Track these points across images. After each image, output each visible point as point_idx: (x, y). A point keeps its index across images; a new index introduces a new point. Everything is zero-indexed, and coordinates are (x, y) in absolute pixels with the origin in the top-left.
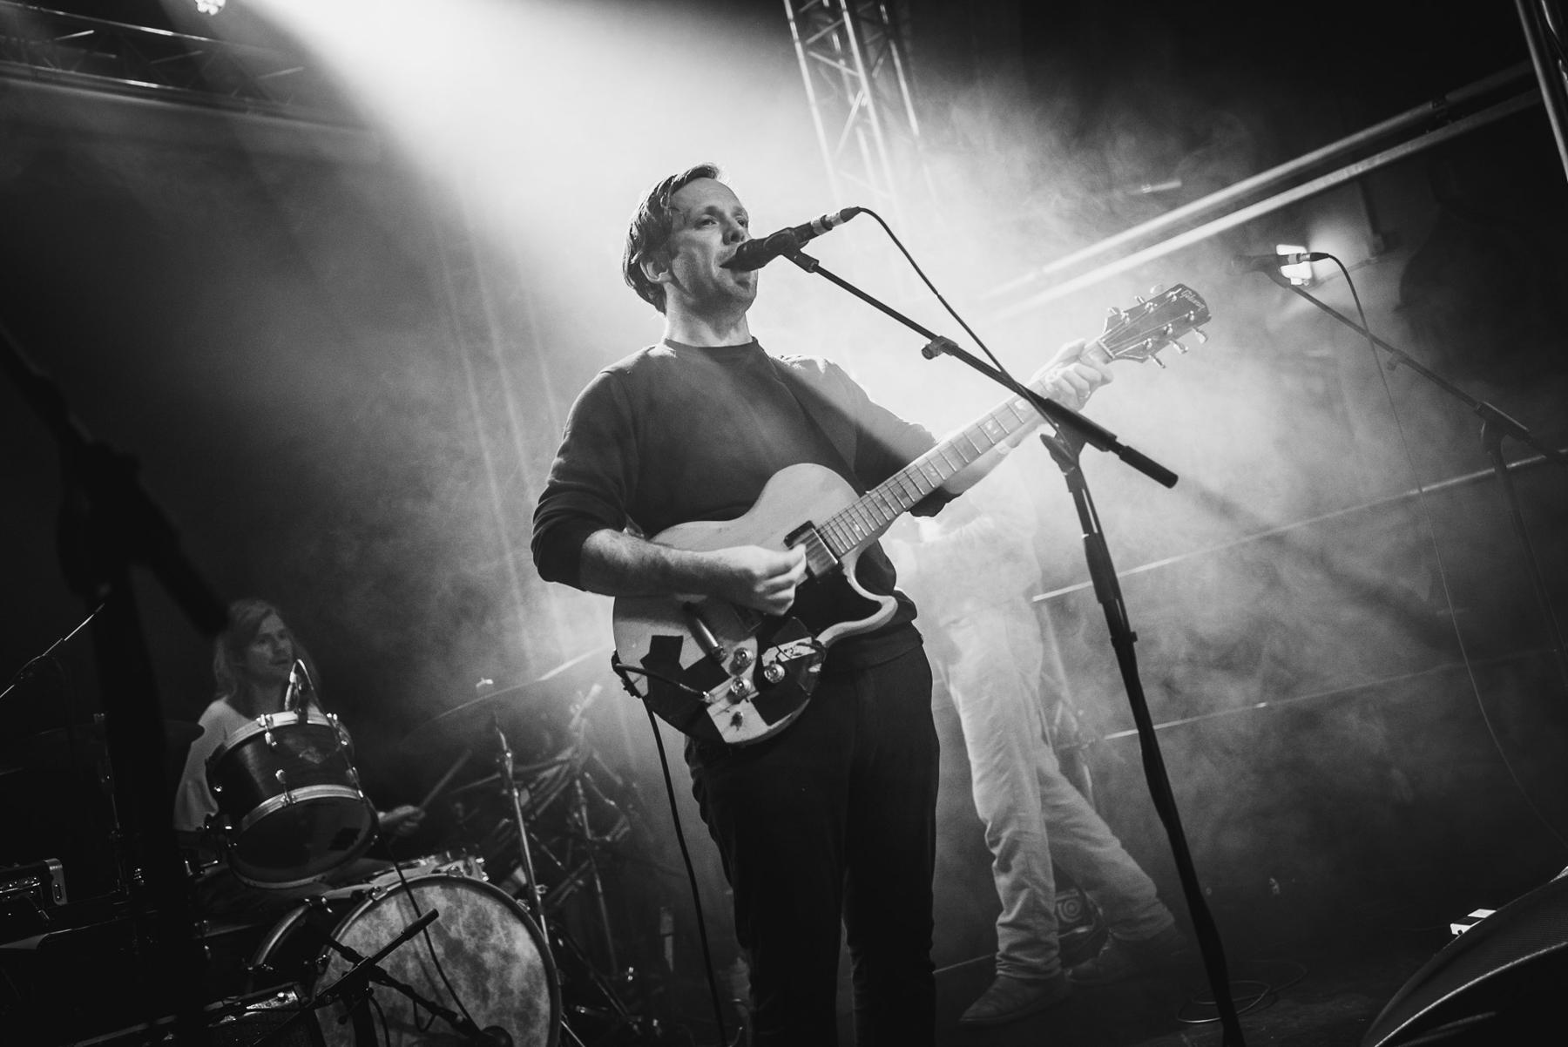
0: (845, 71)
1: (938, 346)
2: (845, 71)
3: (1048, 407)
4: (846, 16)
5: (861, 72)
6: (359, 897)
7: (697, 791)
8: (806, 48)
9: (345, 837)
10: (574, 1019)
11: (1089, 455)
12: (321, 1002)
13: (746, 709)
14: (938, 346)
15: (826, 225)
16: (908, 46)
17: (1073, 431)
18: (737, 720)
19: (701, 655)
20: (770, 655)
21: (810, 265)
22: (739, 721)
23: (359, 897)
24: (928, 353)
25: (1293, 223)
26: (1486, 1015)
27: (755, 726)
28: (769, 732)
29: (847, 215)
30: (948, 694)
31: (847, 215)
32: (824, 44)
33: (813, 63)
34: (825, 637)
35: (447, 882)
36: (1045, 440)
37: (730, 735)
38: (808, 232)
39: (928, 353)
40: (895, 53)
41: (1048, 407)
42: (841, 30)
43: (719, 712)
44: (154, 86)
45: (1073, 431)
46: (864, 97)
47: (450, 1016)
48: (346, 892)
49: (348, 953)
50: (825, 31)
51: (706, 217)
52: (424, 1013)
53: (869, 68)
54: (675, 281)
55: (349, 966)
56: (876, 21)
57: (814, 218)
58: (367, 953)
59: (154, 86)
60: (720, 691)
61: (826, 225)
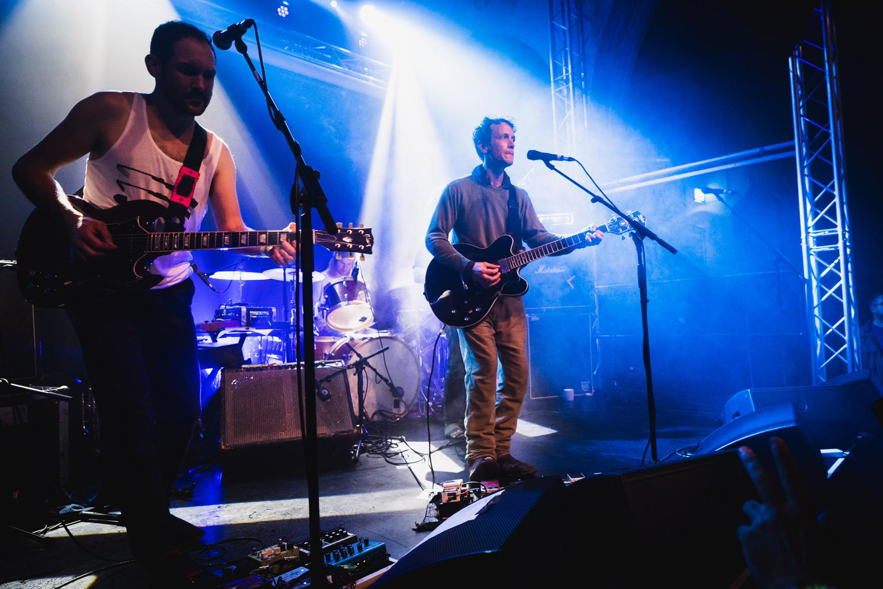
0: (566, 101)
1: (596, 199)
2: (566, 101)
3: (634, 224)
4: (571, 84)
5: (572, 104)
8: (556, 92)
11: (647, 242)
12: (349, 367)
14: (596, 199)
15: (562, 158)
16: (589, 97)
17: (641, 233)
21: (552, 167)
24: (594, 201)
25: (701, 182)
26: (441, 297)
28: (376, 258)
29: (570, 159)
31: (570, 159)
32: (560, 91)
33: (556, 97)
36: (632, 234)
38: (554, 157)
39: (594, 201)
40: (771, 272)
41: (634, 224)
42: (568, 88)
44: (818, 352)
45: (641, 233)
46: (572, 112)
49: (359, 355)
50: (562, 87)
51: (507, 193)
53: (575, 102)
55: (358, 359)
56: (580, 88)
57: (559, 155)
58: (364, 356)
59: (818, 352)
61: (562, 158)
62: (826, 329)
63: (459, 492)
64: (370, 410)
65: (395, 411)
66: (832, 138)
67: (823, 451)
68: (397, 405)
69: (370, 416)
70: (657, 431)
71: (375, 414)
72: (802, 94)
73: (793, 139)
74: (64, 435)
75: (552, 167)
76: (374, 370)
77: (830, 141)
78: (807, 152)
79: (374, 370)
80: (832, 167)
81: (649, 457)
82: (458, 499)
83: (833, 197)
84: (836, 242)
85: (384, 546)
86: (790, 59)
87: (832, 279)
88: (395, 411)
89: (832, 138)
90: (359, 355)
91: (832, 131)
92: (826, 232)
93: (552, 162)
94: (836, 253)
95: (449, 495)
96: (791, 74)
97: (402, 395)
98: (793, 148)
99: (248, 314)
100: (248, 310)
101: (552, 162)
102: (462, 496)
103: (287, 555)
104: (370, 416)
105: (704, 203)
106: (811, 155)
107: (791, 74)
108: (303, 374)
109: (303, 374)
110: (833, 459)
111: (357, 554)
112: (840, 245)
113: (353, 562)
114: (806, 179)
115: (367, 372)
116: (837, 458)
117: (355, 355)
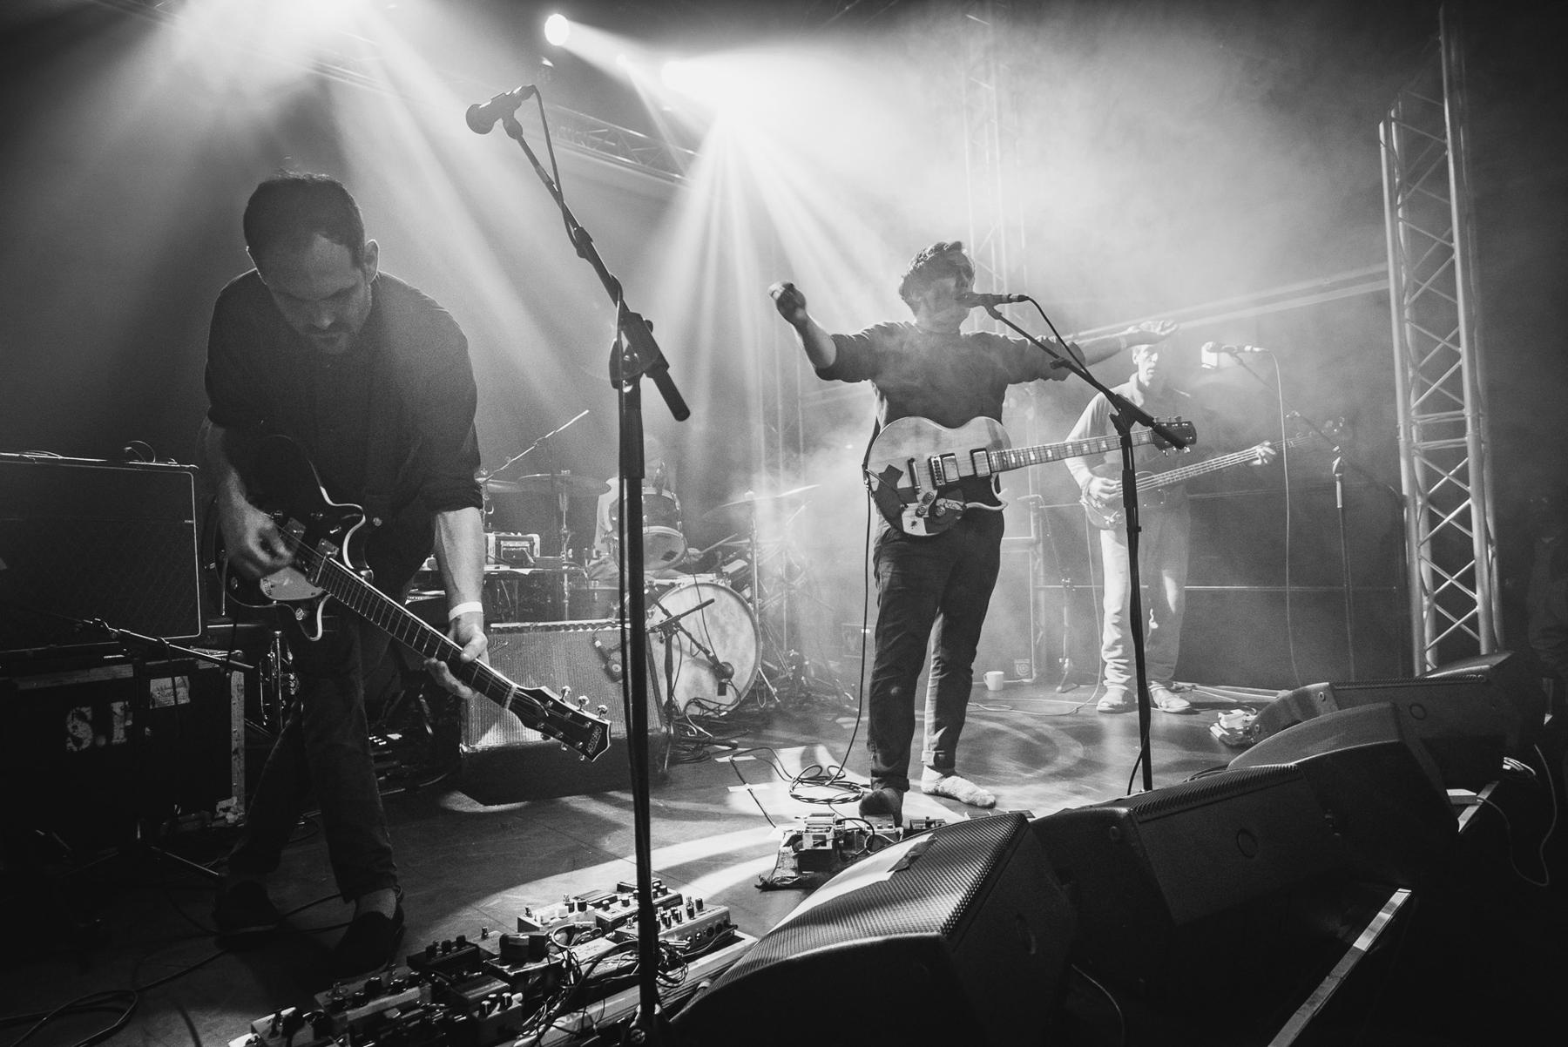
6: (673, 585)
7: (1219, 472)
9: (669, 556)
10: (763, 666)
13: (921, 522)
18: (914, 523)
19: (971, 473)
20: (941, 502)
21: (998, 316)
22: (914, 524)
23: (673, 585)
27: (920, 530)
29: (1022, 298)
30: (1055, 721)
31: (1022, 298)
34: (969, 505)
35: (716, 586)
37: (907, 529)
38: (1000, 300)
43: (907, 518)
47: (707, 652)
48: (667, 582)
49: (665, 612)
52: (696, 649)
54: (925, 301)
55: (664, 618)
58: (674, 614)
60: (912, 507)
62: (1437, 580)
63: (830, 836)
64: (681, 699)
65: (721, 699)
66: (1457, 256)
67: (1451, 792)
68: (722, 692)
69: (682, 707)
70: (652, 801)
71: (689, 703)
72: (1401, 183)
73: (1385, 259)
74: (238, 726)
75: (998, 316)
76: (689, 635)
77: (1453, 262)
78: (1408, 281)
79: (689, 635)
80: (1456, 306)
81: (1138, 788)
82: (829, 846)
83: (1458, 356)
84: (1463, 434)
85: (727, 913)
86: (1381, 126)
87: (1452, 496)
88: (721, 699)
89: (1457, 256)
90: (665, 612)
91: (1456, 244)
92: (1445, 416)
93: (998, 308)
94: (1462, 452)
95: (815, 837)
96: (1383, 150)
97: (730, 676)
98: (1385, 274)
99: (498, 546)
100: (498, 539)
101: (998, 308)
102: (835, 842)
103: (578, 919)
104: (682, 707)
105: (1217, 369)
106: (1417, 287)
107: (1383, 150)
108: (628, 633)
109: (628, 633)
110: (1462, 805)
111: (686, 921)
112: (1469, 438)
113: (682, 934)
114: (1407, 326)
115: (680, 639)
116: (1466, 806)
117: (658, 610)
